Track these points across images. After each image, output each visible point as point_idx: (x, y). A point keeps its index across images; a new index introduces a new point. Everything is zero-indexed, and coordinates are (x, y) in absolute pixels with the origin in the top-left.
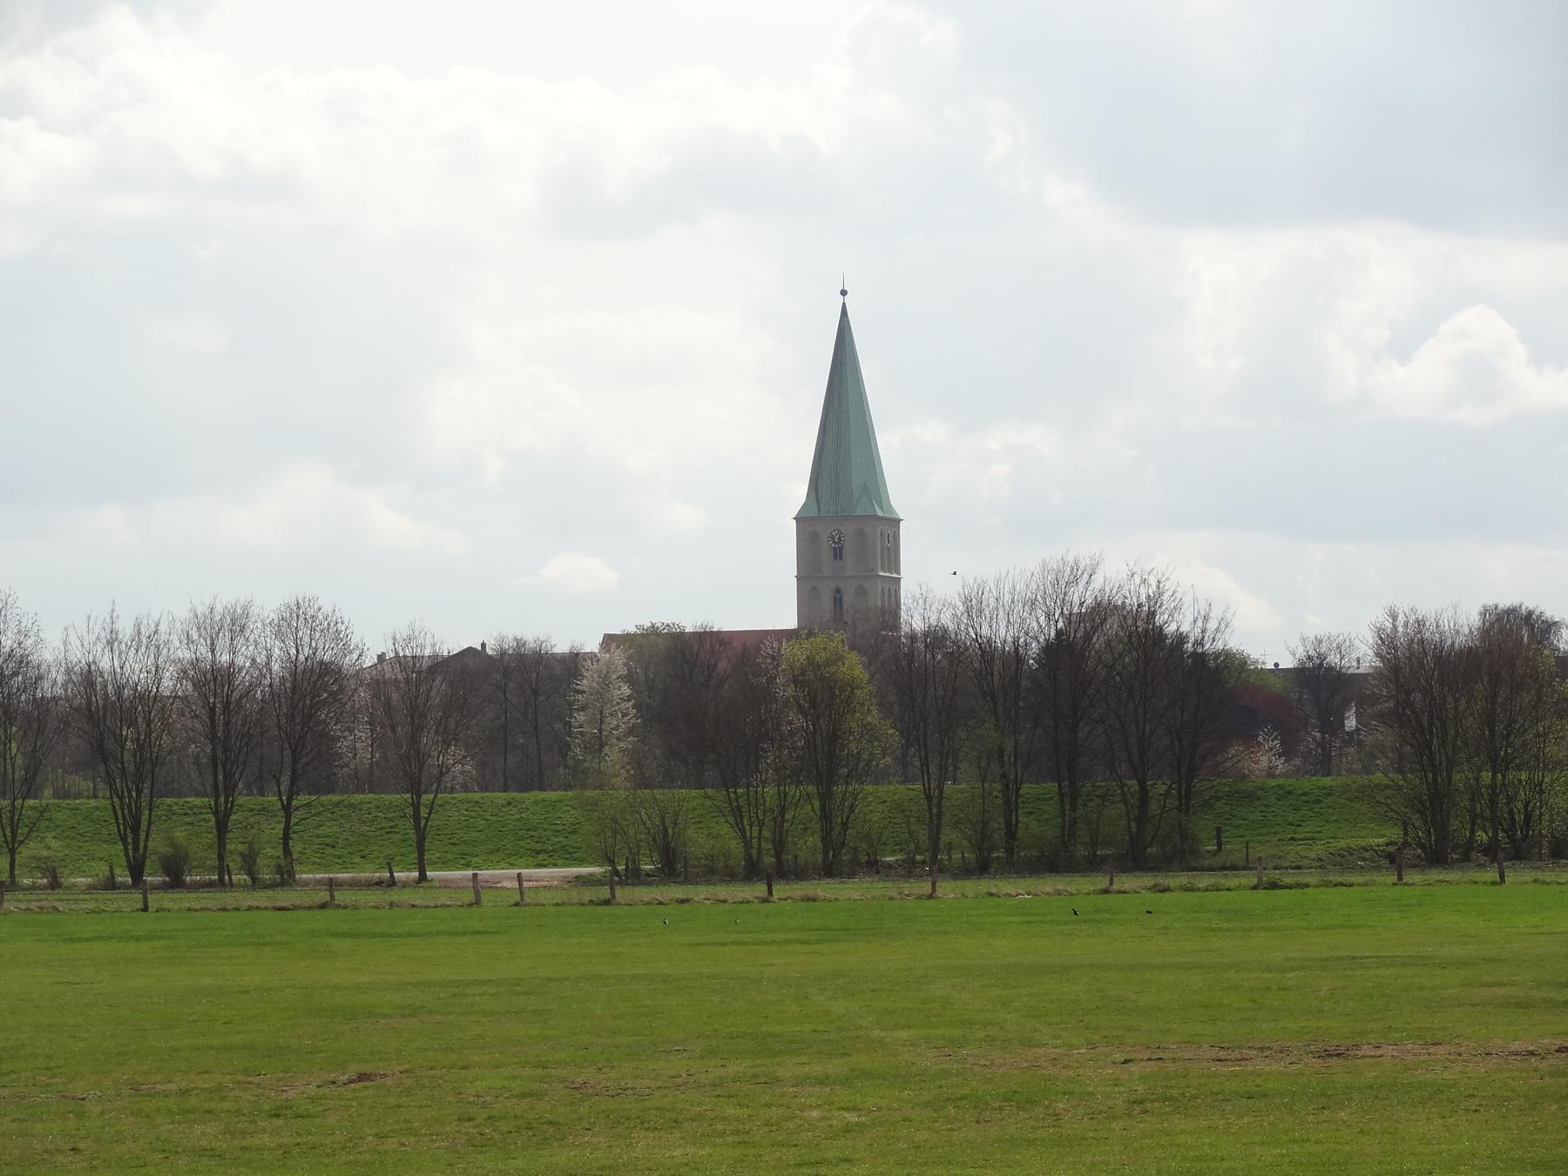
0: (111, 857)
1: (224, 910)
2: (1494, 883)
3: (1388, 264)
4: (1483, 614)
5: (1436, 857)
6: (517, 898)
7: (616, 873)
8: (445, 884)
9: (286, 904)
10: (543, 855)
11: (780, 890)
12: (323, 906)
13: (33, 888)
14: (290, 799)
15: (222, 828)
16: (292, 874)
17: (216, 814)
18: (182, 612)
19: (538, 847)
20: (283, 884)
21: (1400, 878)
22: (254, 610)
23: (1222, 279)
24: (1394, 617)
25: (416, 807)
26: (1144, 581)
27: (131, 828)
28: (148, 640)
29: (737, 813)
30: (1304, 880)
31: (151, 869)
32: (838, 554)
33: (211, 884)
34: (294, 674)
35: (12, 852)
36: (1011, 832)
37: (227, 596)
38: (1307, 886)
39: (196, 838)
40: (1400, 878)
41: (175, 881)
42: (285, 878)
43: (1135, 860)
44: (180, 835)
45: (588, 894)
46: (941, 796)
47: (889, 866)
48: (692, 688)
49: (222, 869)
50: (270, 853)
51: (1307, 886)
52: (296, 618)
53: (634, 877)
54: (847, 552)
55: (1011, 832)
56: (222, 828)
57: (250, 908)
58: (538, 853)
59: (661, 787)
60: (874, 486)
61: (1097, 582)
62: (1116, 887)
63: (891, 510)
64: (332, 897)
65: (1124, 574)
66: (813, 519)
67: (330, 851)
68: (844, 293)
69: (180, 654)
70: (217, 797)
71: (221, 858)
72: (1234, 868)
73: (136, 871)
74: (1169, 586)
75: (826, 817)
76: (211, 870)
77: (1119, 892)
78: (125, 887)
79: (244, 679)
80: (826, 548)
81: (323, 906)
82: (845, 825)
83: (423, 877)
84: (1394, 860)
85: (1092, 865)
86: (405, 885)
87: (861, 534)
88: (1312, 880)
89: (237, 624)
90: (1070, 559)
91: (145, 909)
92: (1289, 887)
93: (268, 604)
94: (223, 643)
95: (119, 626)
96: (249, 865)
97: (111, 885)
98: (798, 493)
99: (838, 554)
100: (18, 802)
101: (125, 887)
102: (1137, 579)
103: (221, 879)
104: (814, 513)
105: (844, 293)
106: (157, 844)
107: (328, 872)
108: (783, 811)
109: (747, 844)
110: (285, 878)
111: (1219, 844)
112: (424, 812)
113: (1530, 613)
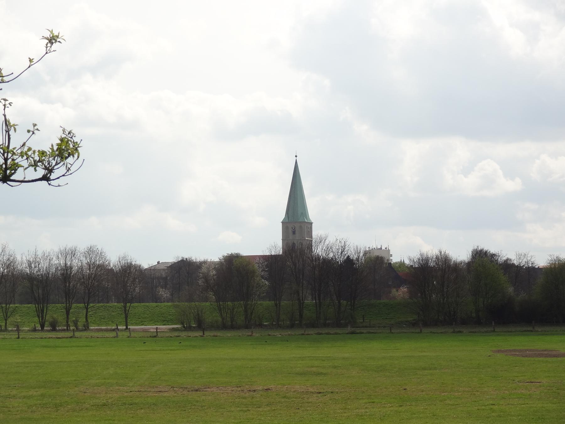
0: (35, 322)
1: (42, 338)
2: (418, 333)
3: (461, 149)
4: (421, 255)
5: (426, 324)
6: (155, 334)
7: (184, 327)
8: (134, 330)
9: (60, 336)
10: (165, 322)
11: (207, 333)
12: (71, 337)
13: (12, 331)
14: (88, 305)
15: (68, 313)
16: (88, 327)
17: (66, 309)
18: (56, 249)
19: (164, 319)
20: (85, 330)
21: (391, 331)
22: (78, 249)
23: (412, 152)
24: (441, 253)
25: (125, 307)
26: (340, 242)
27: (41, 314)
28: (46, 257)
29: (220, 310)
30: (362, 331)
31: (48, 325)
32: (294, 233)
33: (64, 330)
34: (422, 266)
35: (6, 320)
36: (301, 316)
37: (69, 244)
38: (363, 333)
39: (60, 317)
40: (391, 331)
41: (54, 329)
42: (86, 328)
43: (338, 324)
44: (55, 316)
45: (176, 334)
46: (280, 306)
47: (266, 325)
48: (235, 272)
49: (68, 326)
50: (82, 320)
51: (363, 333)
52: (90, 251)
53: (189, 328)
54: (296, 232)
55: (301, 316)
56: (68, 313)
57: (49, 338)
58: (164, 321)
59: (198, 301)
60: (305, 213)
61: (327, 242)
62: (306, 333)
63: (310, 220)
64: (74, 335)
65: (335, 239)
66: (287, 223)
67: (103, 320)
68: (296, 156)
69: (56, 262)
70: (66, 304)
71: (67, 322)
72: (366, 327)
73: (42, 326)
74: (347, 243)
75: (246, 311)
76: (64, 326)
77: (307, 334)
78: (39, 330)
79: (75, 269)
80: (290, 231)
81: (71, 337)
82: (252, 313)
83: (127, 328)
84: (414, 324)
85: (325, 325)
86: (122, 330)
87: (301, 227)
88: (365, 331)
89: (73, 253)
90: (319, 235)
91: (19, 338)
92: (358, 333)
93: (82, 247)
94: (68, 258)
95: (38, 253)
96: (76, 323)
97: (35, 330)
98: (281, 214)
99: (294, 233)
100: (8, 306)
101: (39, 330)
102: (338, 241)
103: (67, 329)
104: (287, 221)
105: (296, 156)
106: (48, 318)
107: (98, 326)
108: (233, 309)
109: (223, 319)
110: (86, 328)
111: (364, 320)
112: (127, 309)
113: (486, 252)
